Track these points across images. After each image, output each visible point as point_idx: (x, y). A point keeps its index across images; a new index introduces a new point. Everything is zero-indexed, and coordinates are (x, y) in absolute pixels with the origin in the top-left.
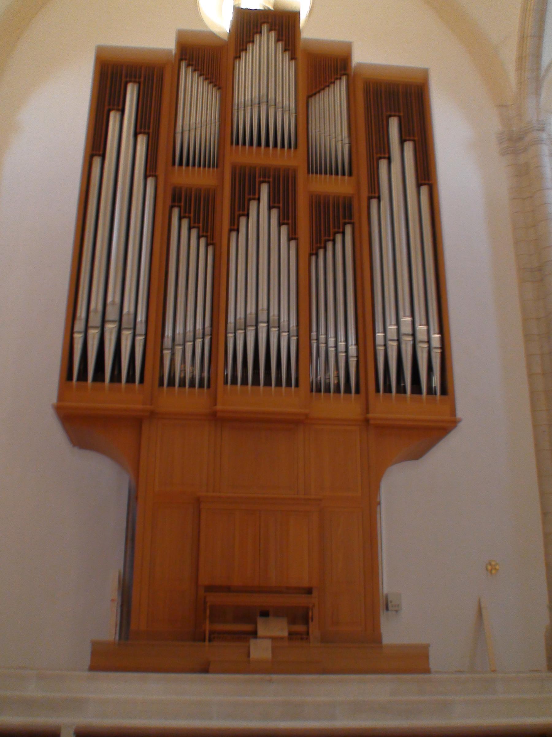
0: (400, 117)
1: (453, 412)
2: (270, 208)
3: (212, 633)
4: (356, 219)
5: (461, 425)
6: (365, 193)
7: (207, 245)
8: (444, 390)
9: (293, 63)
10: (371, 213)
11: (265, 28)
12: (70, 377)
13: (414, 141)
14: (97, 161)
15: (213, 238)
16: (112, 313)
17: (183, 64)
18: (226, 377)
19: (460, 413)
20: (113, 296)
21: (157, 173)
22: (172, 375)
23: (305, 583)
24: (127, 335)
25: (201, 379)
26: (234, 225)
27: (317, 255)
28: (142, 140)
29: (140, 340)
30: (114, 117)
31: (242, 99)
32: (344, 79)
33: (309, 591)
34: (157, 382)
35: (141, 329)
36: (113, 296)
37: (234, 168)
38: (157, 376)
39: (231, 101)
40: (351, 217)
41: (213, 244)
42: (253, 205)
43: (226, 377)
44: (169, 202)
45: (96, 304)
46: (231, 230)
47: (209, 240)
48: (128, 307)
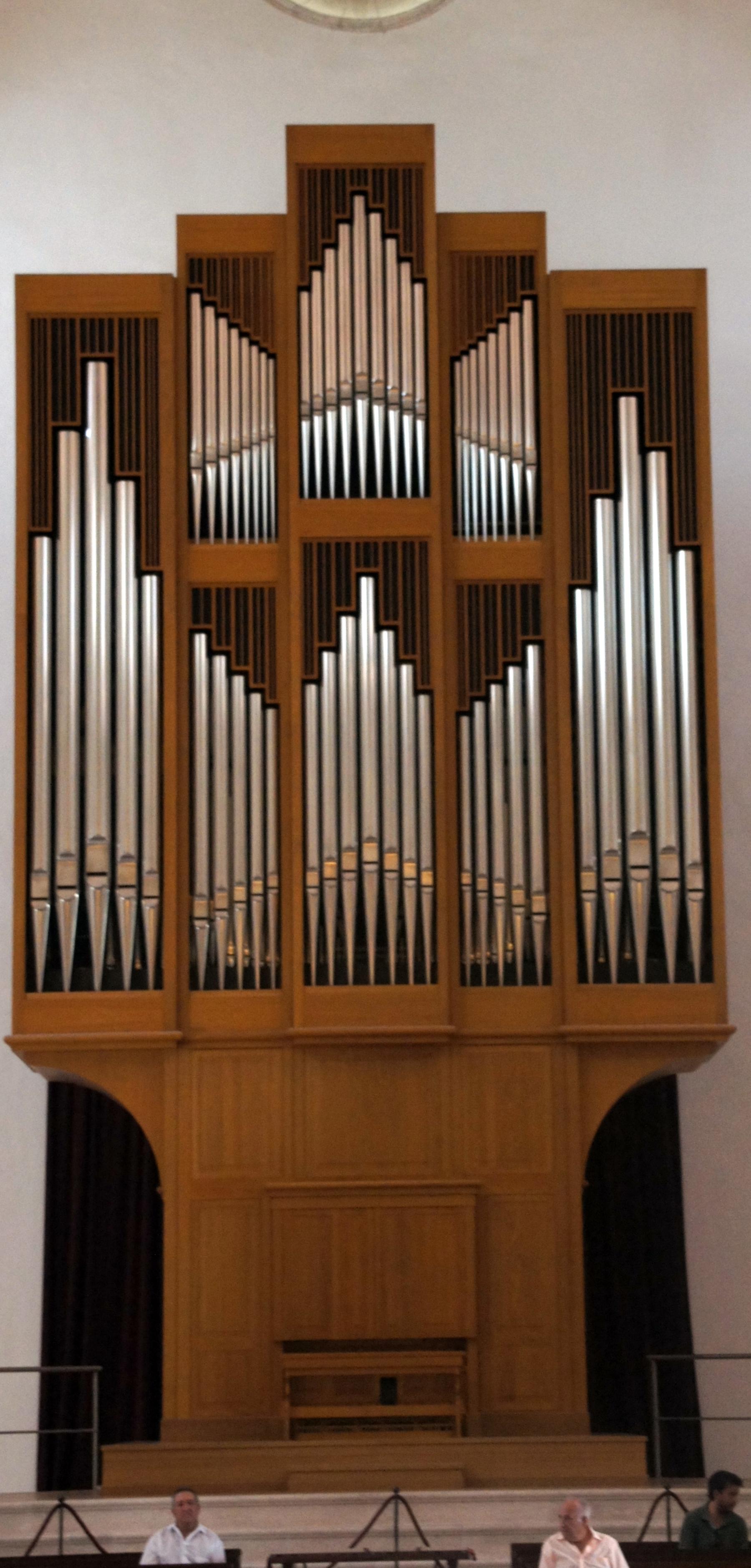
0: (640, 397)
1: (722, 1016)
2: (378, 628)
3: (294, 1422)
4: (546, 632)
5: (730, 1049)
6: (564, 578)
7: (265, 706)
8: (708, 975)
9: (419, 288)
10: (504, 816)
11: (359, 203)
12: (30, 985)
13: (668, 450)
14: (43, 544)
15: (273, 693)
16: (97, 858)
17: (196, 299)
18: (307, 967)
19: (733, 1020)
20: (97, 826)
21: (162, 567)
22: (213, 952)
23: (453, 1331)
24: (126, 900)
25: (265, 970)
26: (312, 672)
27: (471, 714)
28: (126, 490)
29: (149, 908)
30: (67, 441)
31: (318, 390)
32: (528, 305)
33: (458, 1344)
34: (185, 984)
35: (151, 887)
36: (97, 826)
37: (306, 548)
38: (186, 968)
39: (282, 757)
40: (537, 630)
41: (276, 706)
42: (346, 624)
43: (307, 967)
44: (187, 624)
45: (67, 841)
46: (305, 682)
47: (267, 696)
48: (126, 844)
